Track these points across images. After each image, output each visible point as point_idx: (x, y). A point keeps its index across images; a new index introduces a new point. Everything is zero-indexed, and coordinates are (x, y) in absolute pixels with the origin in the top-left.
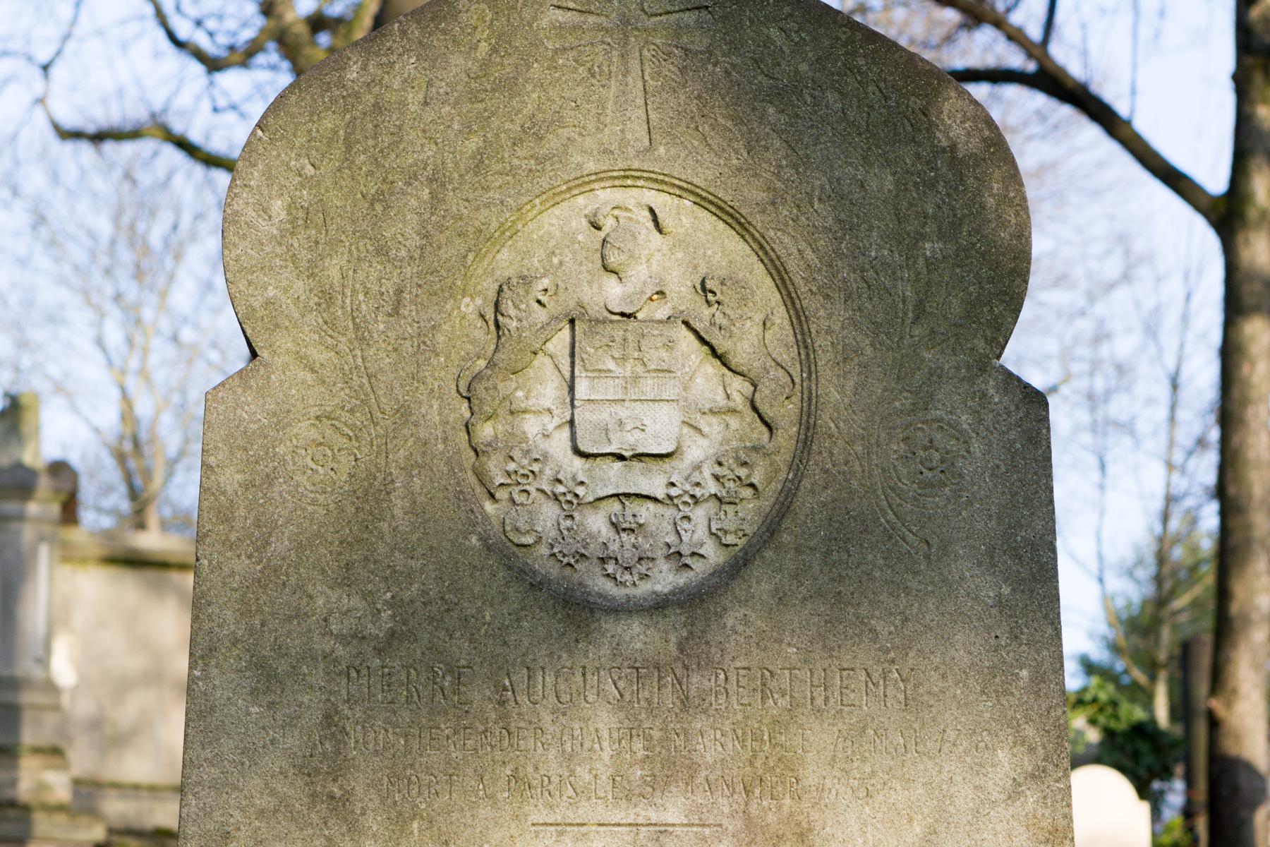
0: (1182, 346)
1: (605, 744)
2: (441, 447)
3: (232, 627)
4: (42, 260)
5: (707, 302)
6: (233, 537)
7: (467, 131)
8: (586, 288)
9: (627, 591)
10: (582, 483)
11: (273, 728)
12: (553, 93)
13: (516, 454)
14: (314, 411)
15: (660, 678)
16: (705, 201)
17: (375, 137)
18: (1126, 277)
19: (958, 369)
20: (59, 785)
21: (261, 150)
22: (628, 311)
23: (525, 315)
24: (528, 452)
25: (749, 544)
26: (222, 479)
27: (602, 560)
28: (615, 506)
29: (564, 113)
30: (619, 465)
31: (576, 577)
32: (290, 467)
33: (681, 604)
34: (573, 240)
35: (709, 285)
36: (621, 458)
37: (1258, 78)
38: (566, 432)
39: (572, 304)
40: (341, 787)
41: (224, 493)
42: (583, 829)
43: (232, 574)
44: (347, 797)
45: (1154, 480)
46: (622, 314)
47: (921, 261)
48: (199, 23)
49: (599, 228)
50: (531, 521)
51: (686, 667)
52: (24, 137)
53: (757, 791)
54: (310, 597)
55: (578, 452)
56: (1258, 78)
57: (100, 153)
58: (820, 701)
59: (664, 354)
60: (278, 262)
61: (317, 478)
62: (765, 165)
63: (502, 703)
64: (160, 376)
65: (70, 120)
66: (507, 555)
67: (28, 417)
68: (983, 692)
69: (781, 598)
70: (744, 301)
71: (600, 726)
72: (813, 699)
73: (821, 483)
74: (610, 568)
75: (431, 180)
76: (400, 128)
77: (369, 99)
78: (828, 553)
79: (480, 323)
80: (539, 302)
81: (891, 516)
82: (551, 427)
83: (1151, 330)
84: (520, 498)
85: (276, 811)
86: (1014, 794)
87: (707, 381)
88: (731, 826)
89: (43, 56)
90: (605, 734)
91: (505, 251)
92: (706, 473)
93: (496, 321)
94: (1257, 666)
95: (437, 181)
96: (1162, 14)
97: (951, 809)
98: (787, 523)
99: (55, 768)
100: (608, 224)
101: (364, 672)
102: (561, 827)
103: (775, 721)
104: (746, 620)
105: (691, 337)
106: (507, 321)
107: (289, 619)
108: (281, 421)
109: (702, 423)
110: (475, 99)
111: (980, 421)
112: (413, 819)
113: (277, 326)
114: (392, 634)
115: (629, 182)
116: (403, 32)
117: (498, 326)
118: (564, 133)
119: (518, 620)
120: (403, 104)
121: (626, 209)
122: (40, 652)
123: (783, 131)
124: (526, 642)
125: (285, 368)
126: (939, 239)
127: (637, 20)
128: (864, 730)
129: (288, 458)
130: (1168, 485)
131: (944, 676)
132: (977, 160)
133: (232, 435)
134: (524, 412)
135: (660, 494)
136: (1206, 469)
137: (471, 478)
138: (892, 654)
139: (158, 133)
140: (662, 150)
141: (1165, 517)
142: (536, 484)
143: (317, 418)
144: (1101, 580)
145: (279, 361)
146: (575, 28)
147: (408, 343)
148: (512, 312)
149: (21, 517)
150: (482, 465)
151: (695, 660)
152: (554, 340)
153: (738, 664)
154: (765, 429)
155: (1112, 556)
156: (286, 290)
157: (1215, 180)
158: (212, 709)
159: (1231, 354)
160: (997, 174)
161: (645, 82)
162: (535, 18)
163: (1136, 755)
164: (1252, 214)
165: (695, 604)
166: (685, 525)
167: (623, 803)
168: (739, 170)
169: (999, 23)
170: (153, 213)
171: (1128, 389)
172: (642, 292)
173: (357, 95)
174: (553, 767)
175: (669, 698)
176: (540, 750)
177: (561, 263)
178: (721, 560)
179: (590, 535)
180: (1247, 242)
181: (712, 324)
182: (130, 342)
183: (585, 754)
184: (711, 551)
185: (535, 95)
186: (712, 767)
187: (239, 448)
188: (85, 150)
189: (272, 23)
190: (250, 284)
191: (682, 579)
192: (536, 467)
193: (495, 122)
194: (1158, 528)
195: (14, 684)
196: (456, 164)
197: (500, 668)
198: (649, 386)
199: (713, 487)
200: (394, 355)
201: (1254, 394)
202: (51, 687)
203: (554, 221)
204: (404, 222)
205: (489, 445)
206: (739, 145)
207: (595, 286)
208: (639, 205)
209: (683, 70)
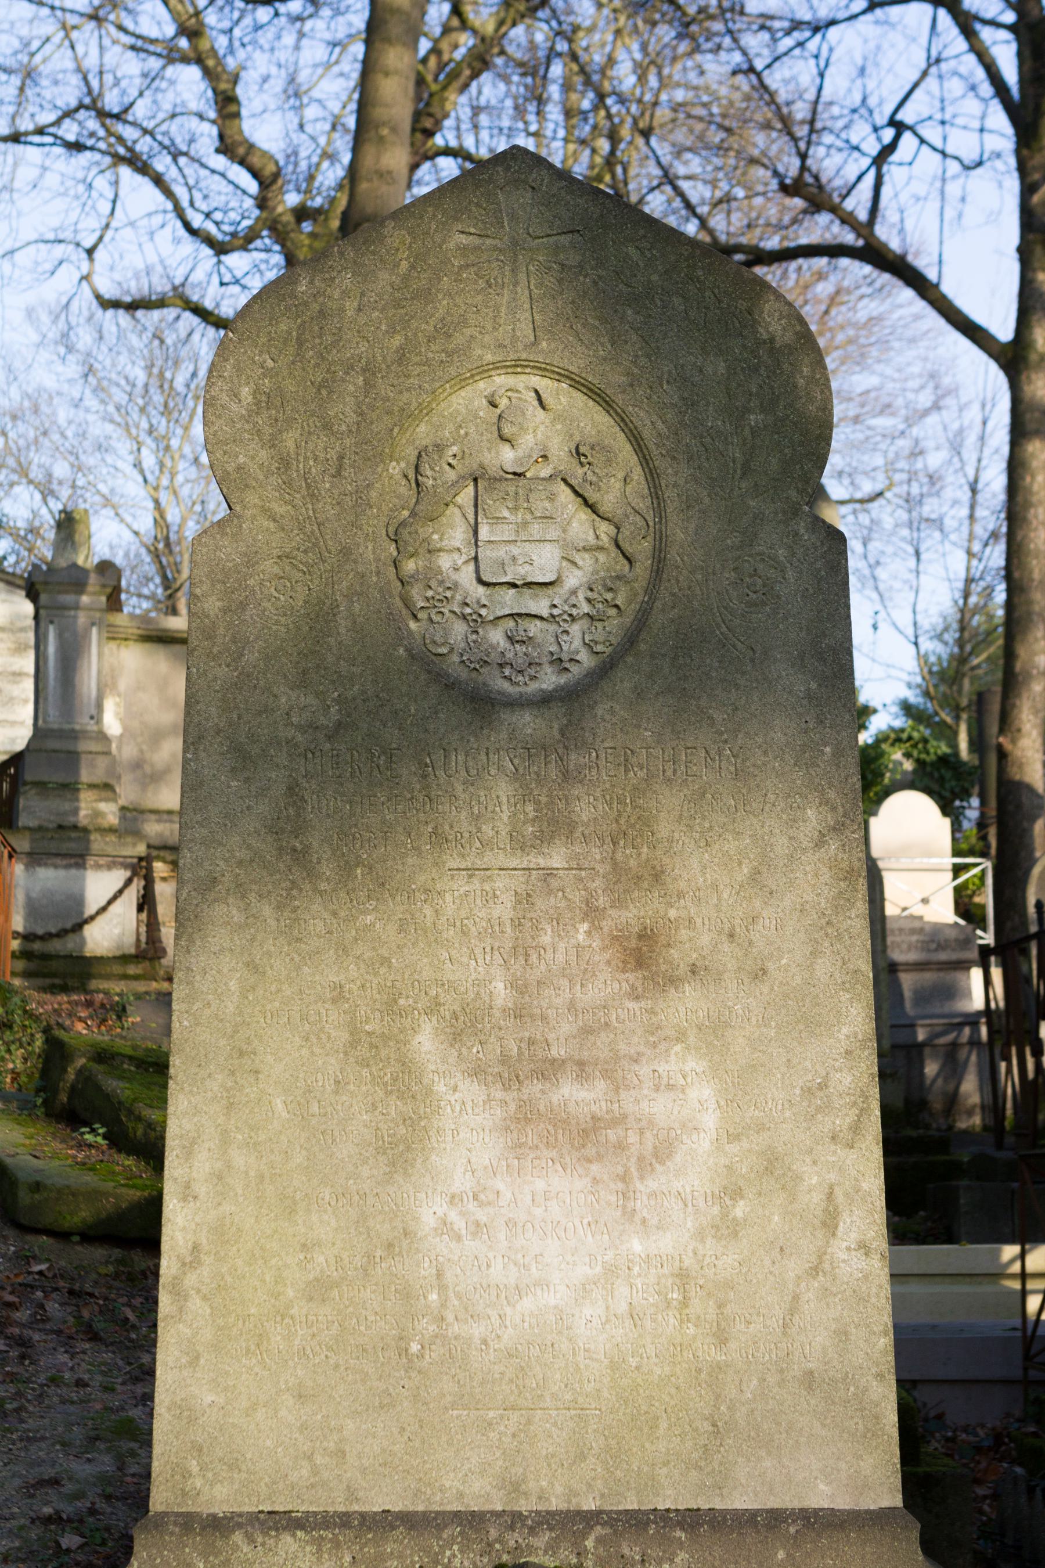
0: (979, 460)
1: (504, 807)
2: (375, 579)
3: (216, 720)
4: (91, 402)
5: (581, 463)
6: (215, 650)
7: (392, 331)
8: (486, 454)
9: (518, 689)
10: (484, 606)
11: (248, 797)
12: (459, 300)
13: (433, 583)
14: (276, 552)
15: (546, 756)
16: (578, 384)
17: (321, 337)
18: (936, 407)
19: (776, 513)
20: (110, 812)
21: (232, 348)
22: (519, 471)
23: (440, 474)
24: (443, 582)
25: (614, 652)
26: (206, 606)
27: (501, 665)
28: (511, 624)
29: (468, 316)
30: (512, 591)
31: (480, 679)
32: (258, 596)
33: (562, 699)
34: (476, 416)
35: (582, 450)
36: (514, 586)
37: (1038, 250)
38: (471, 567)
39: (475, 466)
40: (301, 843)
41: (208, 616)
42: (488, 873)
43: (215, 679)
44: (307, 850)
45: (958, 564)
46: (515, 474)
47: (747, 430)
48: (208, 215)
49: (495, 406)
50: (446, 635)
51: (566, 748)
52: (74, 306)
53: (622, 842)
54: (276, 696)
55: (480, 581)
56: (1038, 250)
57: (133, 317)
58: (669, 773)
59: (547, 504)
60: (247, 436)
61: (279, 604)
62: (625, 356)
63: (425, 776)
64: (185, 491)
65: (108, 291)
66: (426, 662)
67: (80, 528)
68: (796, 764)
69: (640, 693)
70: (609, 462)
71: (501, 793)
72: (664, 771)
73: (670, 604)
74: (507, 672)
75: (364, 370)
76: (340, 329)
77: (315, 307)
78: (675, 658)
79: (404, 482)
80: (449, 464)
81: (724, 629)
82: (460, 562)
83: (956, 449)
84: (436, 618)
85: (252, 861)
86: (820, 843)
87: (581, 525)
88: (601, 869)
89: (88, 243)
90: (504, 800)
91: (423, 425)
92: (581, 596)
93: (417, 480)
94: (1036, 712)
96: (963, 199)
97: (772, 855)
98: (643, 635)
99: (106, 800)
100: (503, 403)
101: (318, 754)
102: (471, 872)
103: (635, 789)
104: (612, 711)
105: (568, 491)
106: (425, 480)
107: (260, 713)
108: (251, 560)
109: (578, 558)
110: (397, 304)
111: (793, 554)
112: (357, 866)
113: (247, 486)
114: (339, 724)
115: (519, 370)
116: (341, 254)
117: (418, 484)
118: (468, 332)
119: (436, 713)
120: (342, 310)
121: (517, 391)
122: (93, 711)
123: (639, 329)
124: (442, 730)
125: (253, 518)
126: (761, 412)
127: (524, 242)
128: (704, 795)
129: (257, 588)
130: (968, 569)
131: (765, 753)
133: (213, 571)
134: (439, 550)
135: (545, 613)
136: (997, 556)
137: (399, 604)
138: (725, 736)
139: (179, 302)
140: (544, 344)
141: (966, 595)
142: (449, 607)
143: (279, 557)
144: (916, 644)
145: (248, 513)
146: (476, 248)
147: (348, 498)
148: (429, 473)
149: (77, 607)
150: (407, 592)
151: (573, 742)
152: (462, 495)
153: (607, 745)
154: (626, 562)
155: (925, 623)
156: (253, 458)
157: (1004, 330)
158: (201, 784)
159: (1016, 467)
160: (806, 360)
161: (530, 291)
162: (444, 241)
163: (942, 780)
164: (1033, 357)
165: (573, 698)
166: (565, 637)
167: (519, 852)
168: (605, 359)
169: (835, 210)
170: (176, 363)
171: (938, 494)
172: (530, 456)
173: (306, 304)
174: (464, 824)
175: (554, 773)
176: (454, 813)
177: (467, 434)
178: (593, 664)
179: (492, 646)
180: (1030, 381)
181: (585, 480)
182: (162, 465)
183: (489, 815)
184: (583, 656)
185: (445, 302)
186: (587, 825)
187: (219, 581)
188: (123, 317)
189: (265, 215)
190: (225, 453)
191: (563, 680)
192: (448, 594)
193: (414, 324)
194: (961, 602)
195: (74, 735)
196: (384, 357)
197: (423, 750)
198: (536, 530)
199: (586, 608)
200: (337, 508)
201: (1034, 499)
202: (103, 737)
203: (461, 401)
204: (345, 404)
205: (412, 577)
206: (605, 340)
207: (493, 452)
208: (527, 388)
209: (560, 281)
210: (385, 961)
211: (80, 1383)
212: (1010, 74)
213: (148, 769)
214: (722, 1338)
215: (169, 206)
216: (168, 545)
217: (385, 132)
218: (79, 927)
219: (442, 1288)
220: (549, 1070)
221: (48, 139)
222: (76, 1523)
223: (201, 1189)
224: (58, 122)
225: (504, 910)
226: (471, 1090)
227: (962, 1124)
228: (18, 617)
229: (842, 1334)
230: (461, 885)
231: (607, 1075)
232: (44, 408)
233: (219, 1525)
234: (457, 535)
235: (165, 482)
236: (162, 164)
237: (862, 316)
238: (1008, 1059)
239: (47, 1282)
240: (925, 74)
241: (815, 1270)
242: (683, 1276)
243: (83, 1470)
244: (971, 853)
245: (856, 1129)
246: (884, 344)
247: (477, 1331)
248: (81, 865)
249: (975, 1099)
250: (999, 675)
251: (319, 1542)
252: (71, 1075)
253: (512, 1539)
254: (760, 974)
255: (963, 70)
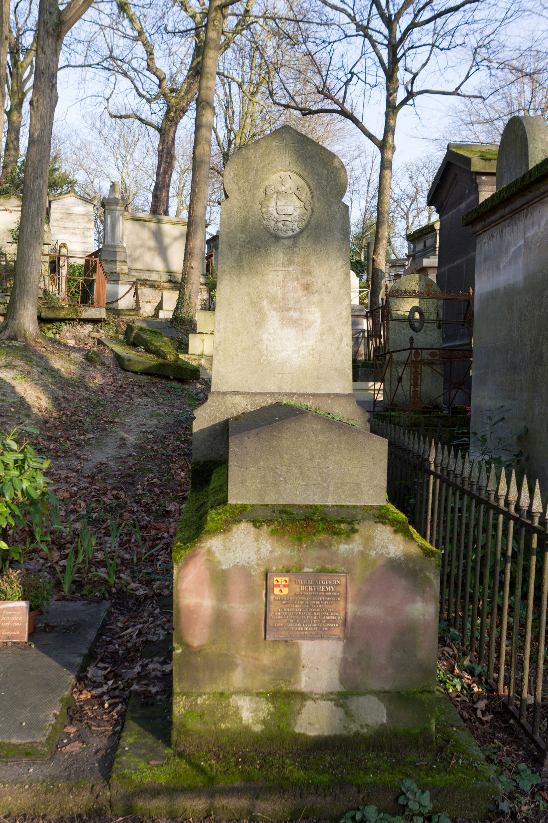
7: (261, 162)
16: (298, 174)
18: (359, 156)
20: (125, 269)
44: (243, 266)
45: (363, 204)
66: (267, 229)
69: (308, 237)
86: (342, 267)
87: (297, 203)
89: (107, 97)
95: (256, 170)
102: (274, 271)
132: (340, 169)
136: (375, 202)
157: (380, 137)
164: (388, 145)
165: (295, 237)
174: (273, 262)
175: (291, 252)
184: (297, 229)
195: (115, 247)
198: (289, 203)
210: (257, 288)
211: (145, 405)
212: (386, 61)
213: (133, 257)
214: (320, 361)
215: (133, 87)
216: (126, 190)
217: (209, 75)
218: (117, 301)
219: (267, 350)
220: (289, 309)
221: (100, 67)
222: (151, 433)
223: (221, 331)
224: (103, 62)
225: (281, 278)
226: (273, 313)
227: (359, 359)
228: (88, 211)
229: (342, 361)
230: (273, 273)
231: (300, 311)
232: (88, 147)
233: (224, 394)
234: (273, 204)
235: (125, 171)
236: (132, 74)
237: (337, 127)
238: (372, 341)
239: (133, 383)
240: (361, 58)
241: (338, 349)
242: (313, 350)
243: (150, 422)
244: (364, 287)
245: (347, 322)
246: (344, 137)
247: (274, 359)
248: (117, 284)
249: (363, 352)
250: (374, 238)
251: (243, 397)
252: (134, 334)
253: (279, 397)
254: (329, 292)
255: (372, 57)
